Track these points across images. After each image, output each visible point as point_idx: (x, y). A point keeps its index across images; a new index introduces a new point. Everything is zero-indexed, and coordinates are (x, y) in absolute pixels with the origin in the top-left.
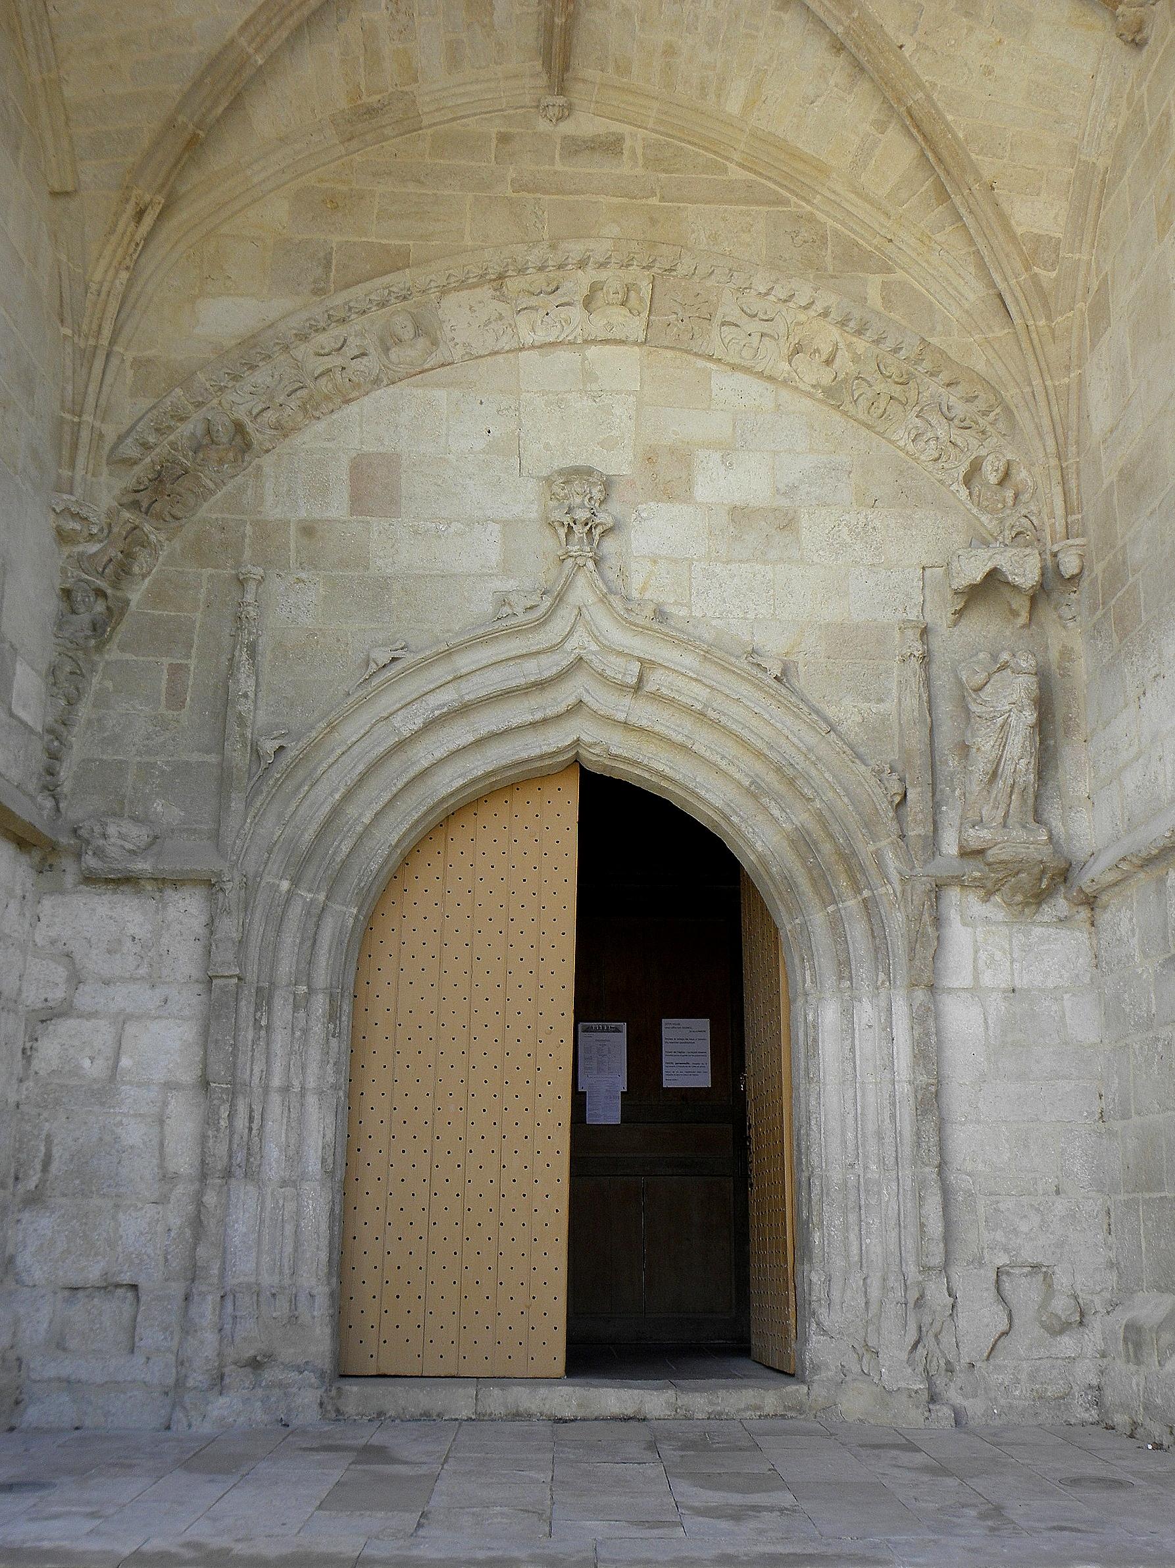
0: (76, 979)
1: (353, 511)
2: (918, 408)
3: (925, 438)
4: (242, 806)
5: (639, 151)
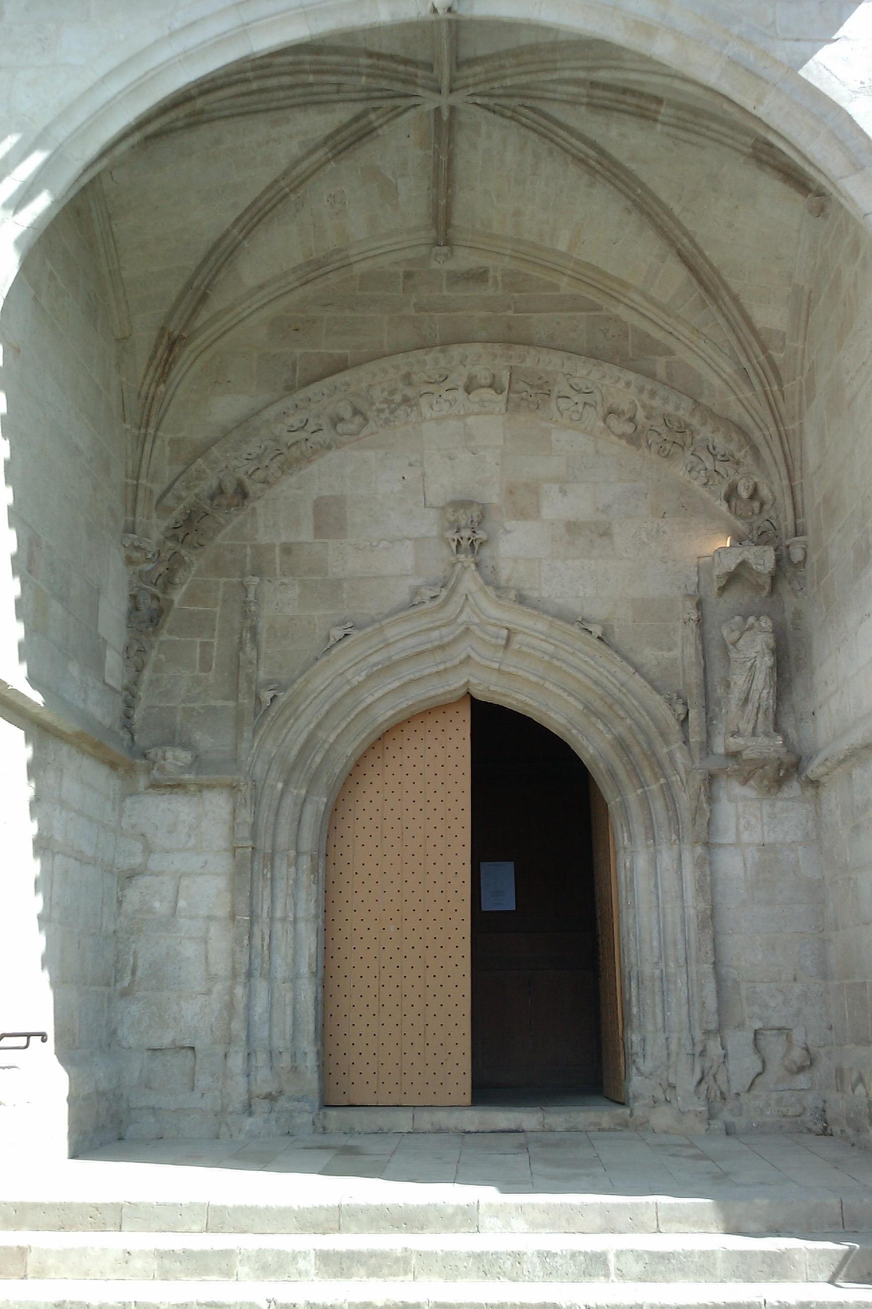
0: (148, 850)
2: (692, 448)
3: (697, 469)
4: (250, 735)
5: (499, 278)
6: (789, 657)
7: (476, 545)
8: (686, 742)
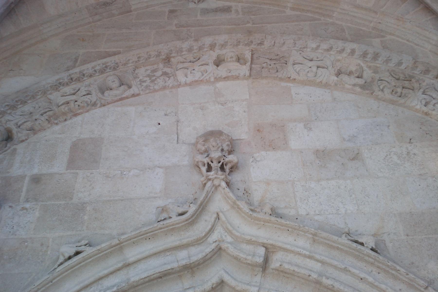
1: (68, 168)
2: (422, 90)
7: (227, 168)
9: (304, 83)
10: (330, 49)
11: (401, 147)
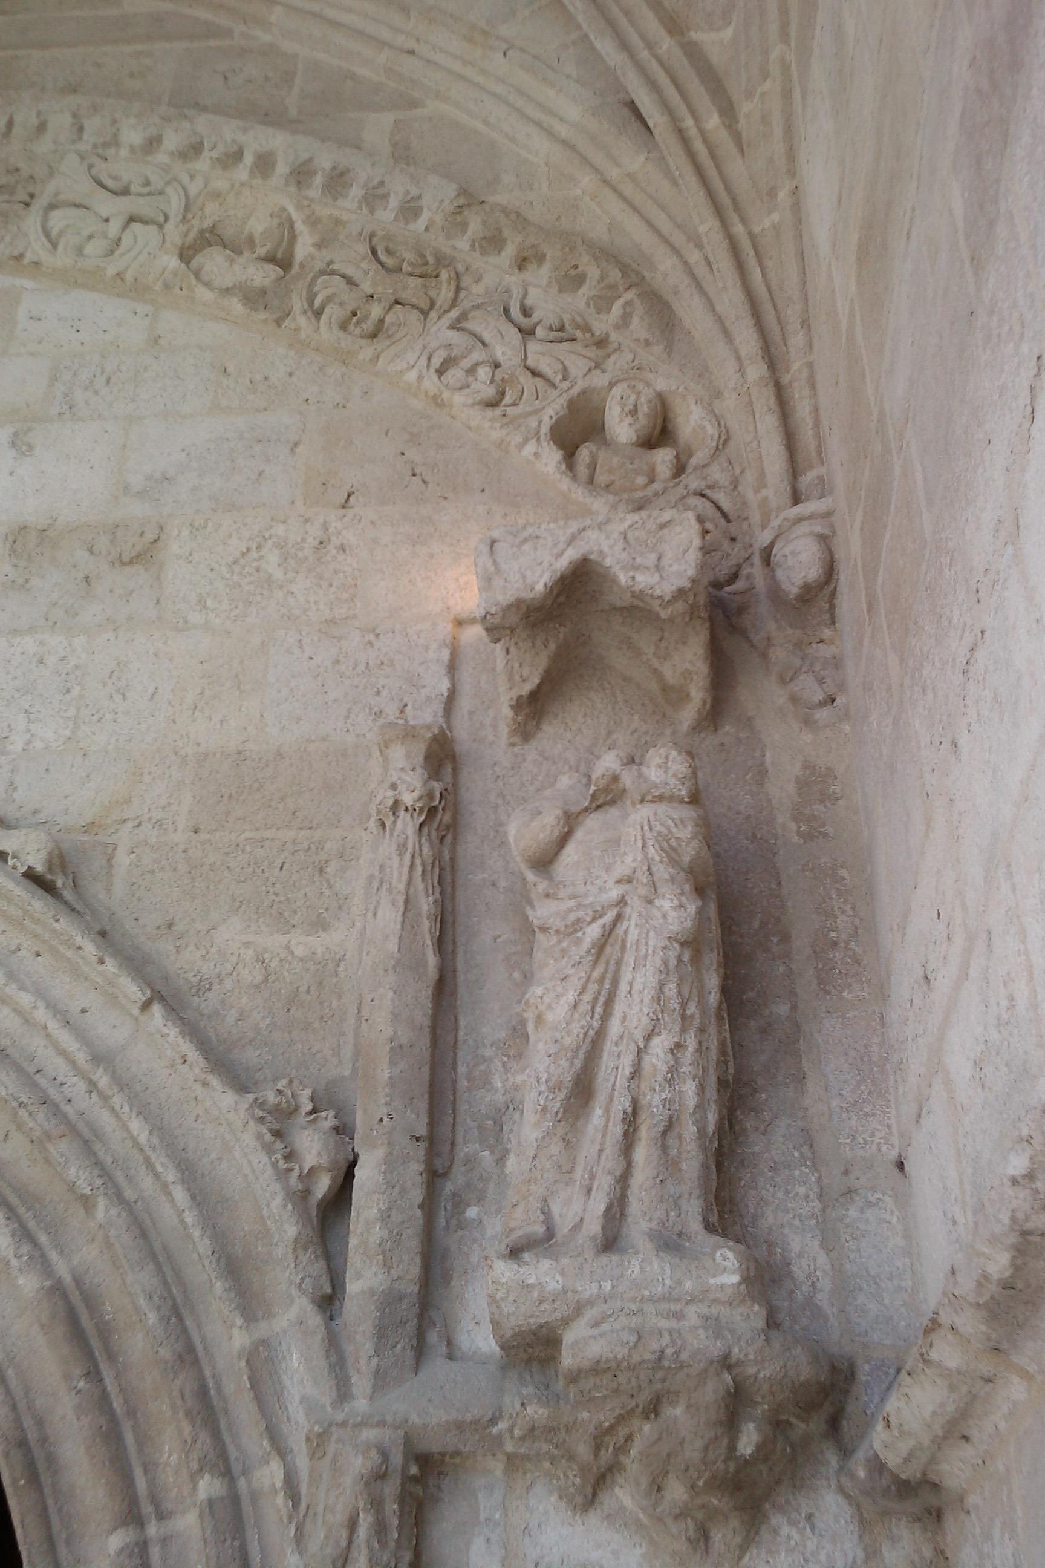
2: (454, 313)
6: (786, 938)
8: (329, 1302)
9: (74, 279)
10: (196, 149)
11: (307, 521)
